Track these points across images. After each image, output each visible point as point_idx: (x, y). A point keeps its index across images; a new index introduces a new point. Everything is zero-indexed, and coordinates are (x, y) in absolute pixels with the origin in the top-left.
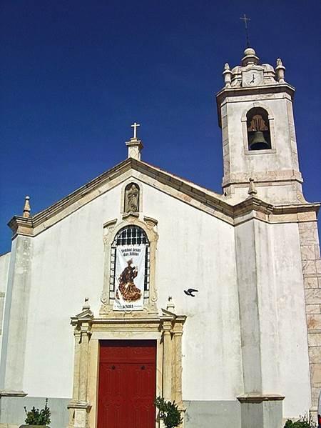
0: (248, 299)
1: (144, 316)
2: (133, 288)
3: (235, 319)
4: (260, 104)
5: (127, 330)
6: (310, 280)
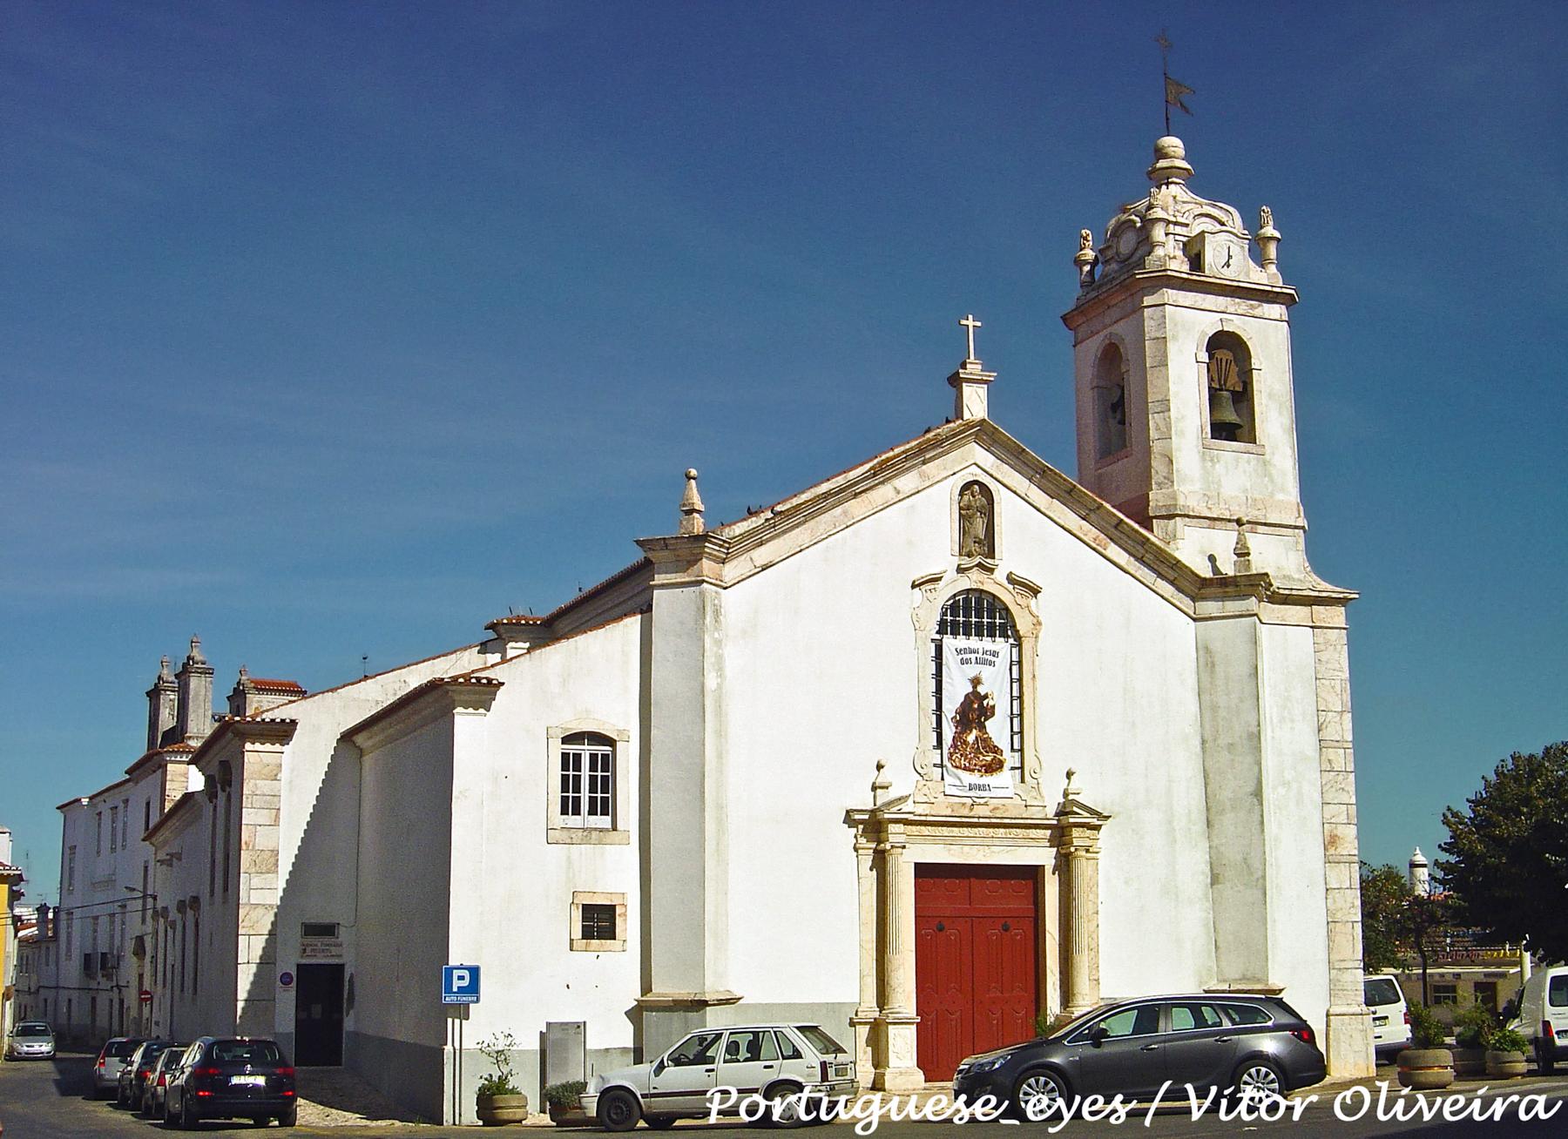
0: (1232, 786)
1: (1014, 810)
4: (1235, 325)
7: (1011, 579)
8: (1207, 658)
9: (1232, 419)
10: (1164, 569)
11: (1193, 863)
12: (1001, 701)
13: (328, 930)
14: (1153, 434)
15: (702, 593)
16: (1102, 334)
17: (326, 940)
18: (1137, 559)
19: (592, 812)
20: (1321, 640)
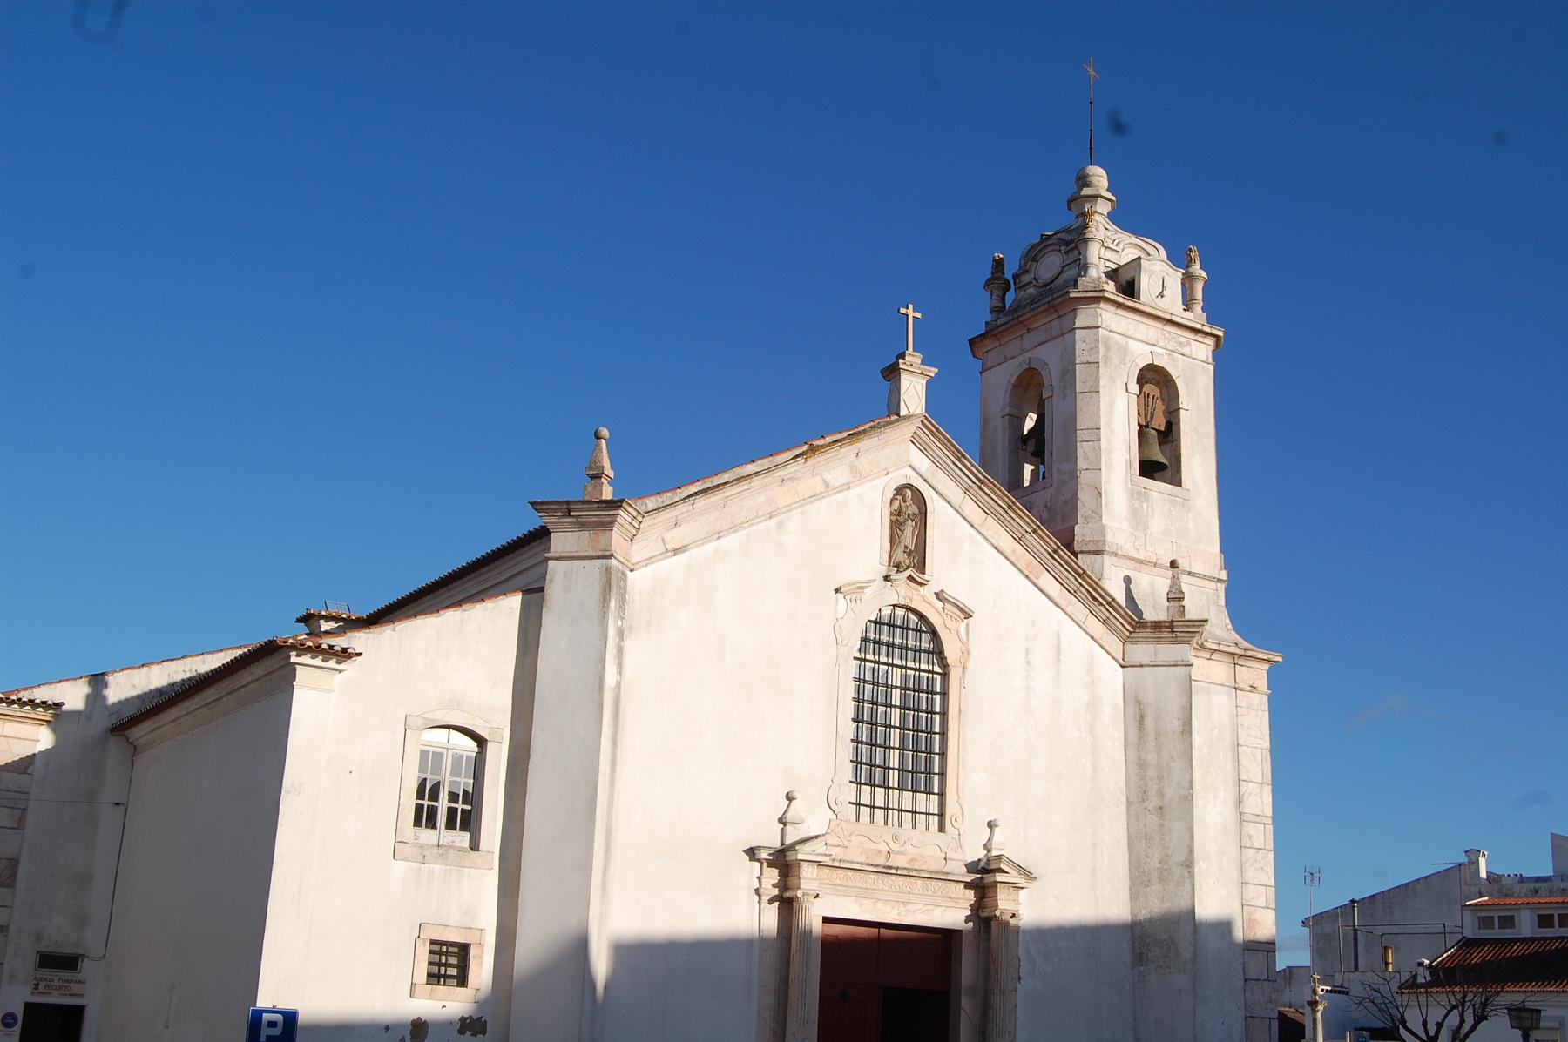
8: (1138, 714)
9: (1159, 464)
13: (69, 962)
14: (1081, 464)
15: (608, 570)
16: (1021, 358)
17: (67, 974)
19: (451, 825)
20: (1243, 704)
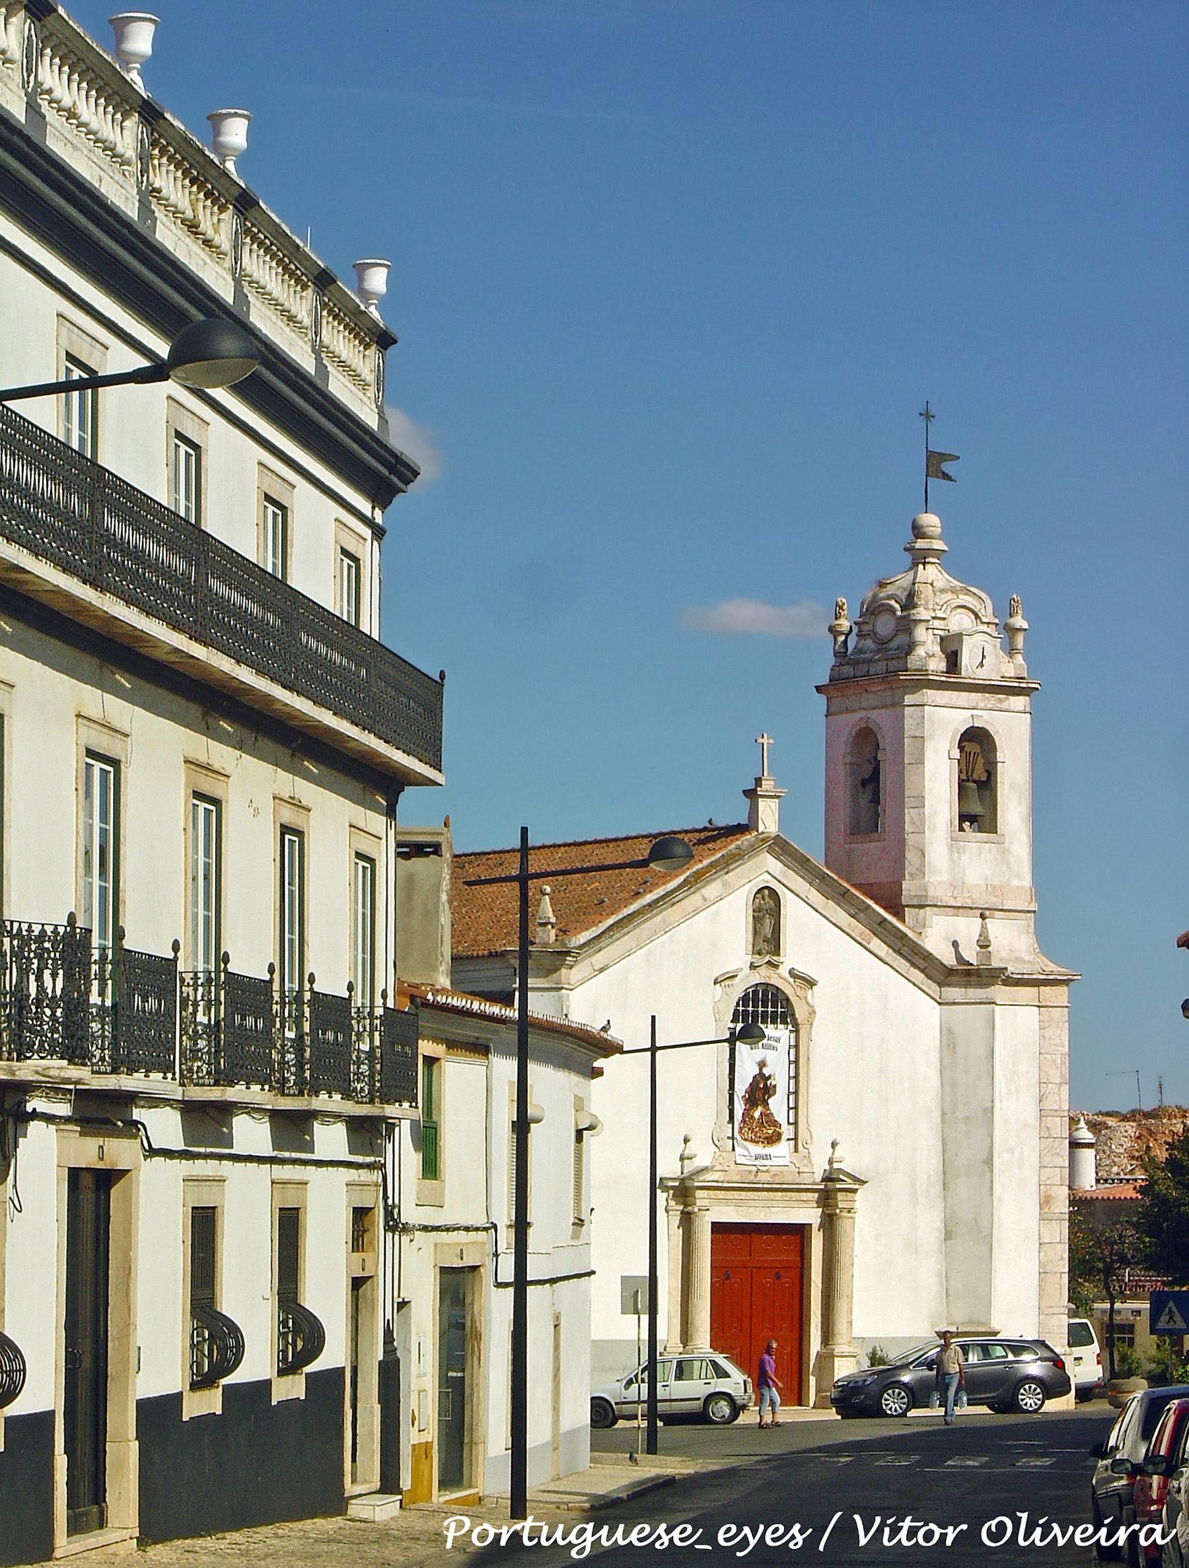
1: (790, 1177)
2: (768, 1119)
3: (937, 1190)
5: (761, 1204)
6: (1049, 1121)
7: (792, 973)
8: (949, 1040)
10: (916, 959)
11: (930, 1222)
12: (781, 1083)
14: (908, 827)
15: (560, 998)
18: (894, 951)
